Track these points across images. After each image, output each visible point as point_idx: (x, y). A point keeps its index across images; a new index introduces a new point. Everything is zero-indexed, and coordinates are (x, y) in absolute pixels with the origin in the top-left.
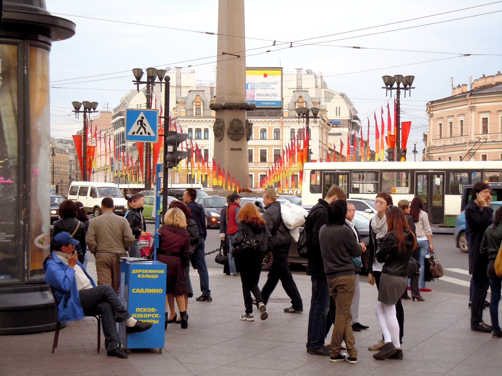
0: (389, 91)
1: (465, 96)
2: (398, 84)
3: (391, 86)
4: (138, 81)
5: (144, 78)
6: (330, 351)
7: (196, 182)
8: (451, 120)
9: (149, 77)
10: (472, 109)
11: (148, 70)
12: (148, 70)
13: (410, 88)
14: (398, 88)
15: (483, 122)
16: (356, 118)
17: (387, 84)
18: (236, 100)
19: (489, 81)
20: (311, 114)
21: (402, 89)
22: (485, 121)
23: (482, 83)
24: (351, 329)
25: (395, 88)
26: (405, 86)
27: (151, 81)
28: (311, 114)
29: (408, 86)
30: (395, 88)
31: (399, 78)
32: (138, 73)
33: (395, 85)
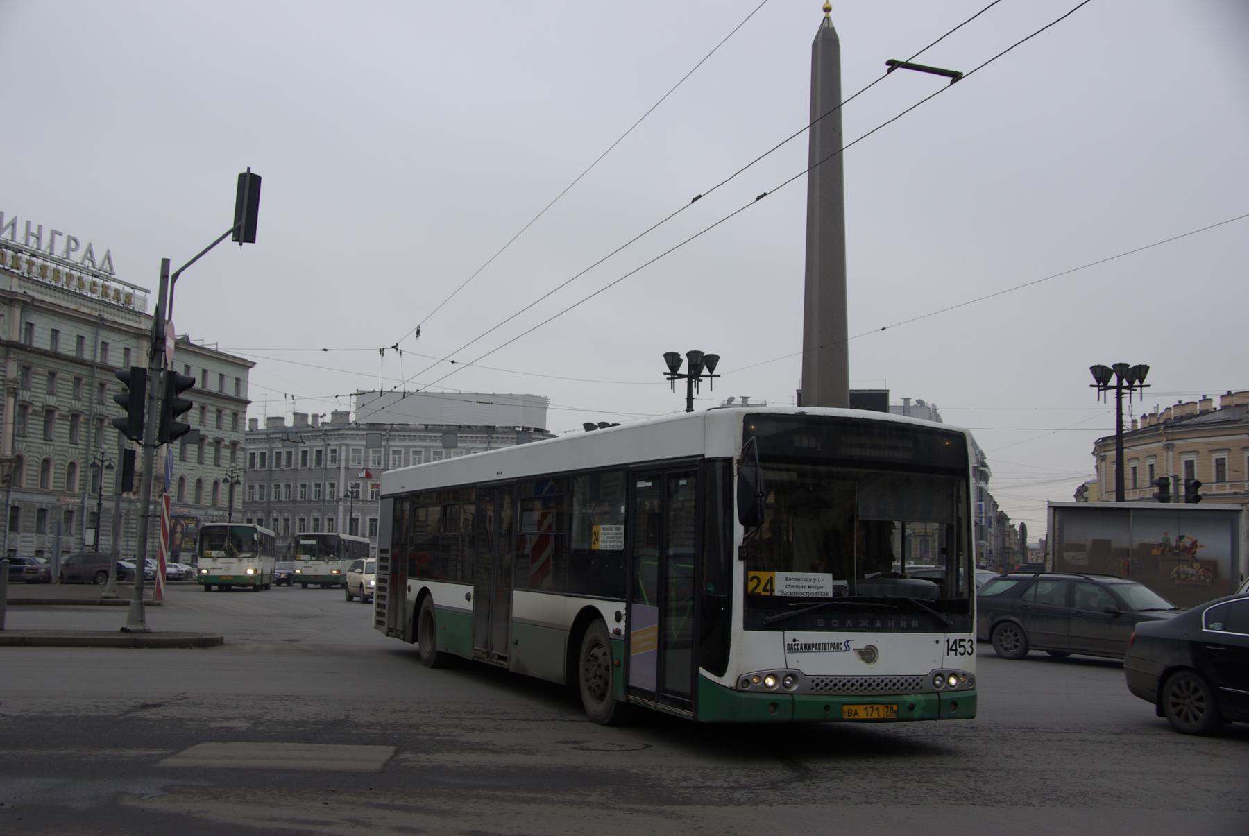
0: (1102, 393)
1: (1157, 430)
2: (1120, 380)
3: (1106, 382)
4: (673, 374)
5: (684, 369)
6: (757, 537)
7: (134, 489)
8: (1151, 461)
9: (691, 367)
10: (1168, 447)
11: (689, 354)
12: (689, 354)
13: (1141, 386)
14: (1119, 387)
15: (1218, 465)
16: (984, 465)
17: (1098, 380)
19: (1188, 410)
21: (1126, 388)
22: (1220, 463)
23: (1179, 412)
24: (873, 665)
25: (682, 376)
26: (1131, 383)
27: (694, 376)
29: (1137, 383)
30: (682, 376)
31: (1121, 369)
32: (672, 360)
33: (1113, 381)
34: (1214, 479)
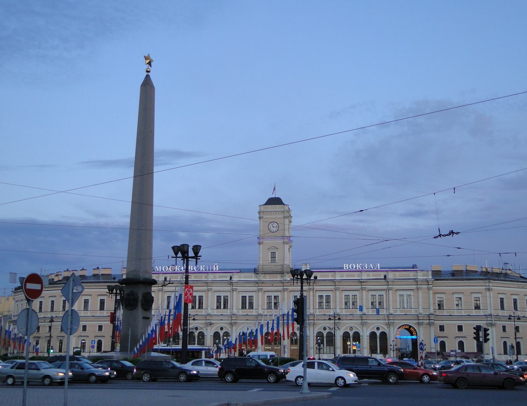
8: (53, 299)
15: (85, 302)
18: (142, 276)
20: (191, 254)
28: (191, 254)
34: (99, 309)
